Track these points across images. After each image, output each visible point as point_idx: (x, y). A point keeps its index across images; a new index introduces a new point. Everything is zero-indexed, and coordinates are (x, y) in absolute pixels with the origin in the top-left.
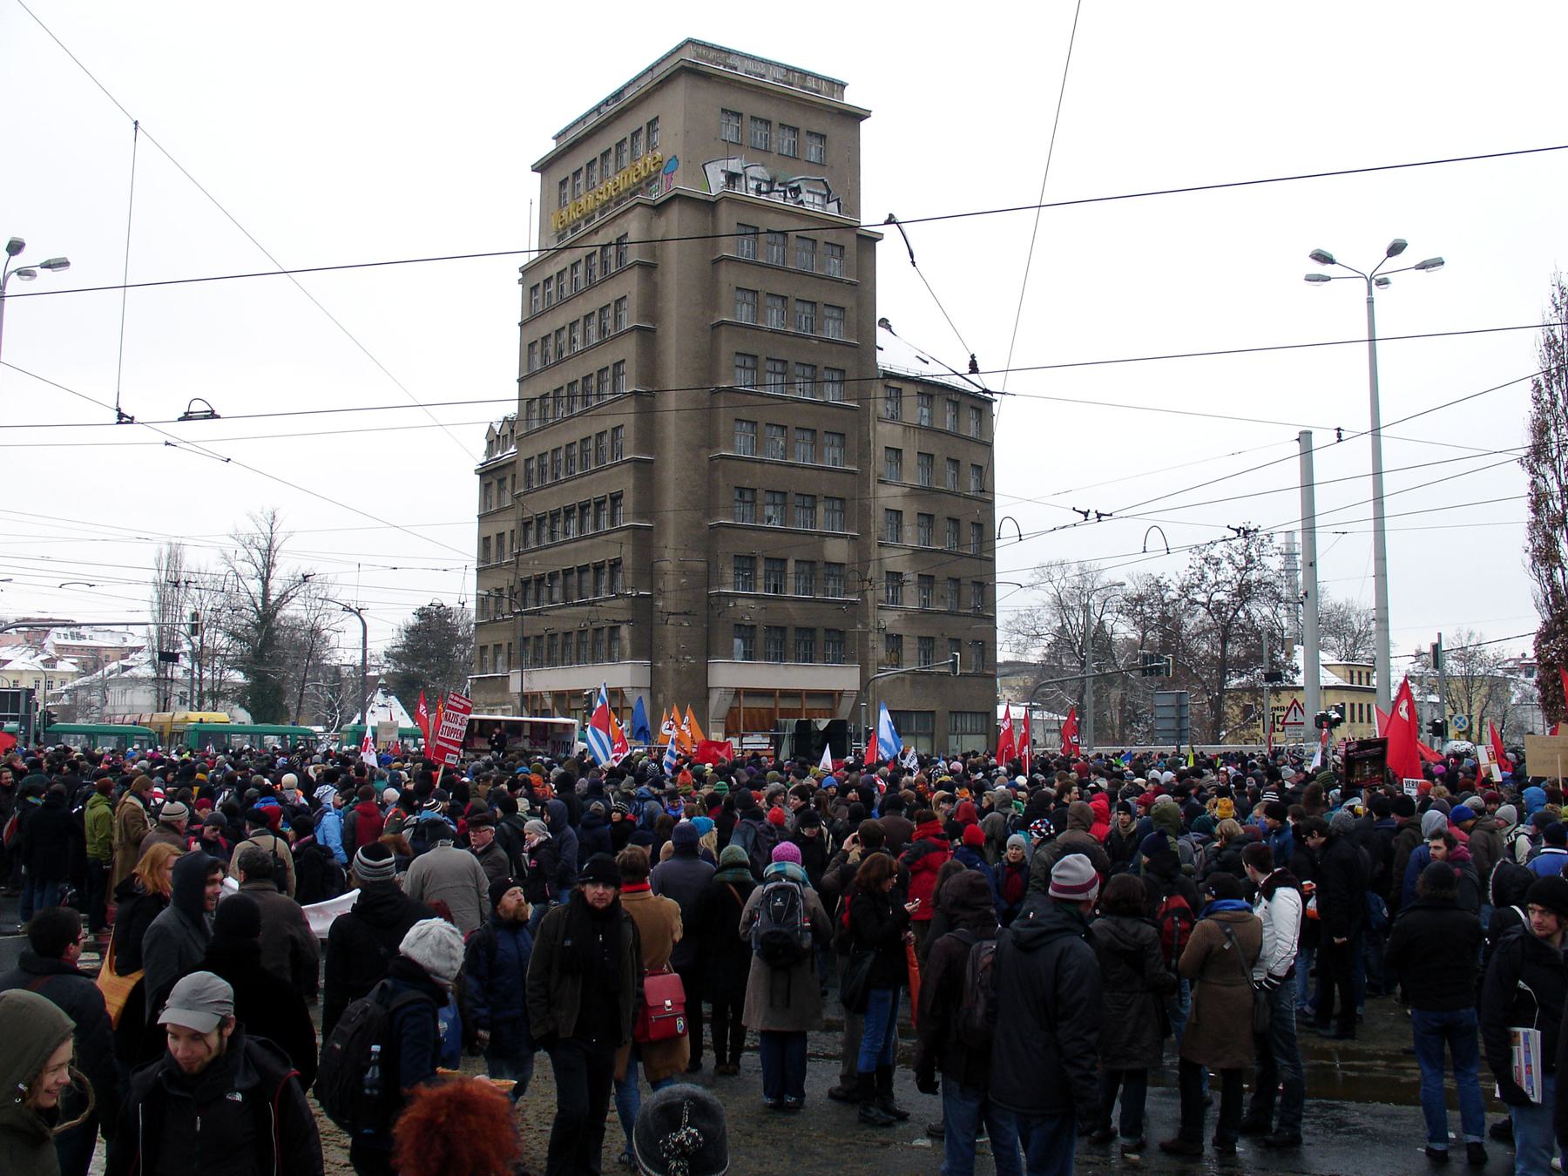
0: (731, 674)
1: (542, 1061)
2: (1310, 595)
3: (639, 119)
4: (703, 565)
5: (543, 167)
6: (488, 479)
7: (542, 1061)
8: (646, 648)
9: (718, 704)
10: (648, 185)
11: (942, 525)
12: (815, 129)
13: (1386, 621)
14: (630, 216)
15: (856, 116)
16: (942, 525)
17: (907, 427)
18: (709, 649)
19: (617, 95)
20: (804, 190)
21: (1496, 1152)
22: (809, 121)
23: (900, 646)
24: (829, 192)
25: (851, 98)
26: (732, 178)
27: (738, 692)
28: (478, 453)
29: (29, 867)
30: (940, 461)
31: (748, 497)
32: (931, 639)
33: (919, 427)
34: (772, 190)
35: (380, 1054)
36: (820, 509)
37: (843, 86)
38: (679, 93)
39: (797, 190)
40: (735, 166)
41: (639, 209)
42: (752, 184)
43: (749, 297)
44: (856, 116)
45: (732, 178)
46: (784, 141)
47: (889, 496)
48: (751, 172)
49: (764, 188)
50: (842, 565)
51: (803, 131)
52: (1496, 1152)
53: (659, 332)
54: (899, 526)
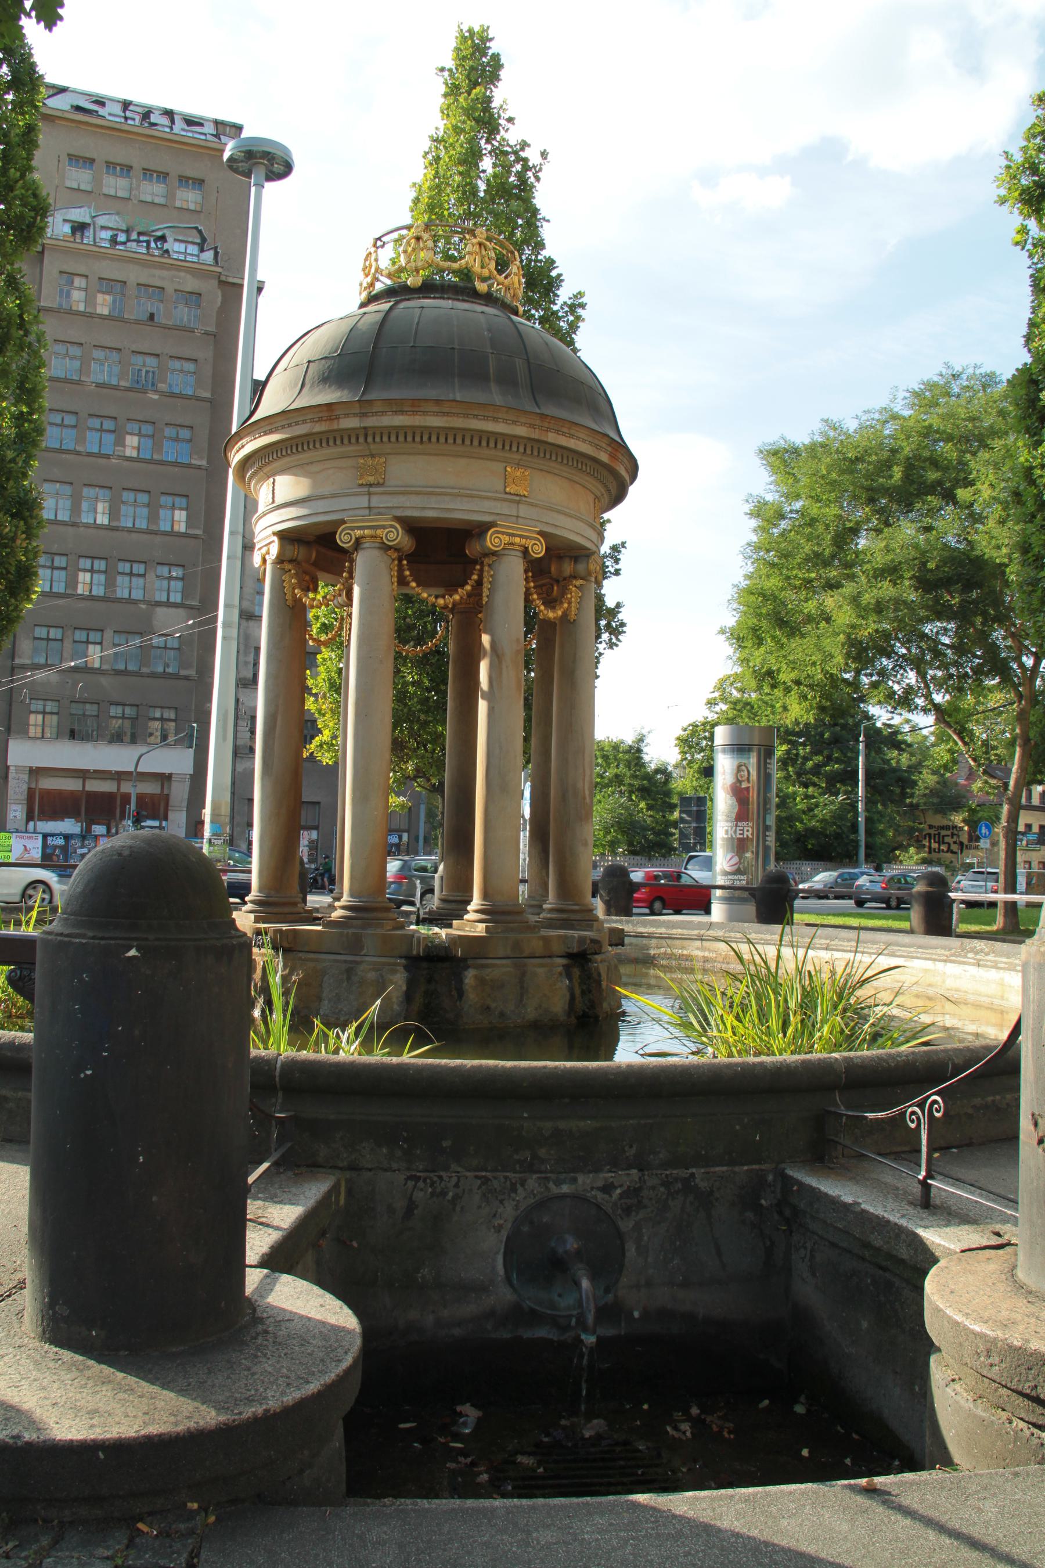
1: (459, 1408)
2: (605, 578)
7: (459, 1408)
12: (189, 173)
13: (118, 773)
20: (170, 239)
21: (3, 1315)
22: (498, 54)
24: (204, 240)
26: (79, 228)
27: (35, 772)
29: (98, 1458)
34: (129, 240)
35: (796, 1402)
39: (163, 239)
40: (80, 215)
42: (106, 235)
43: (115, 355)
48: (102, 221)
49: (122, 238)
52: (3, 1315)
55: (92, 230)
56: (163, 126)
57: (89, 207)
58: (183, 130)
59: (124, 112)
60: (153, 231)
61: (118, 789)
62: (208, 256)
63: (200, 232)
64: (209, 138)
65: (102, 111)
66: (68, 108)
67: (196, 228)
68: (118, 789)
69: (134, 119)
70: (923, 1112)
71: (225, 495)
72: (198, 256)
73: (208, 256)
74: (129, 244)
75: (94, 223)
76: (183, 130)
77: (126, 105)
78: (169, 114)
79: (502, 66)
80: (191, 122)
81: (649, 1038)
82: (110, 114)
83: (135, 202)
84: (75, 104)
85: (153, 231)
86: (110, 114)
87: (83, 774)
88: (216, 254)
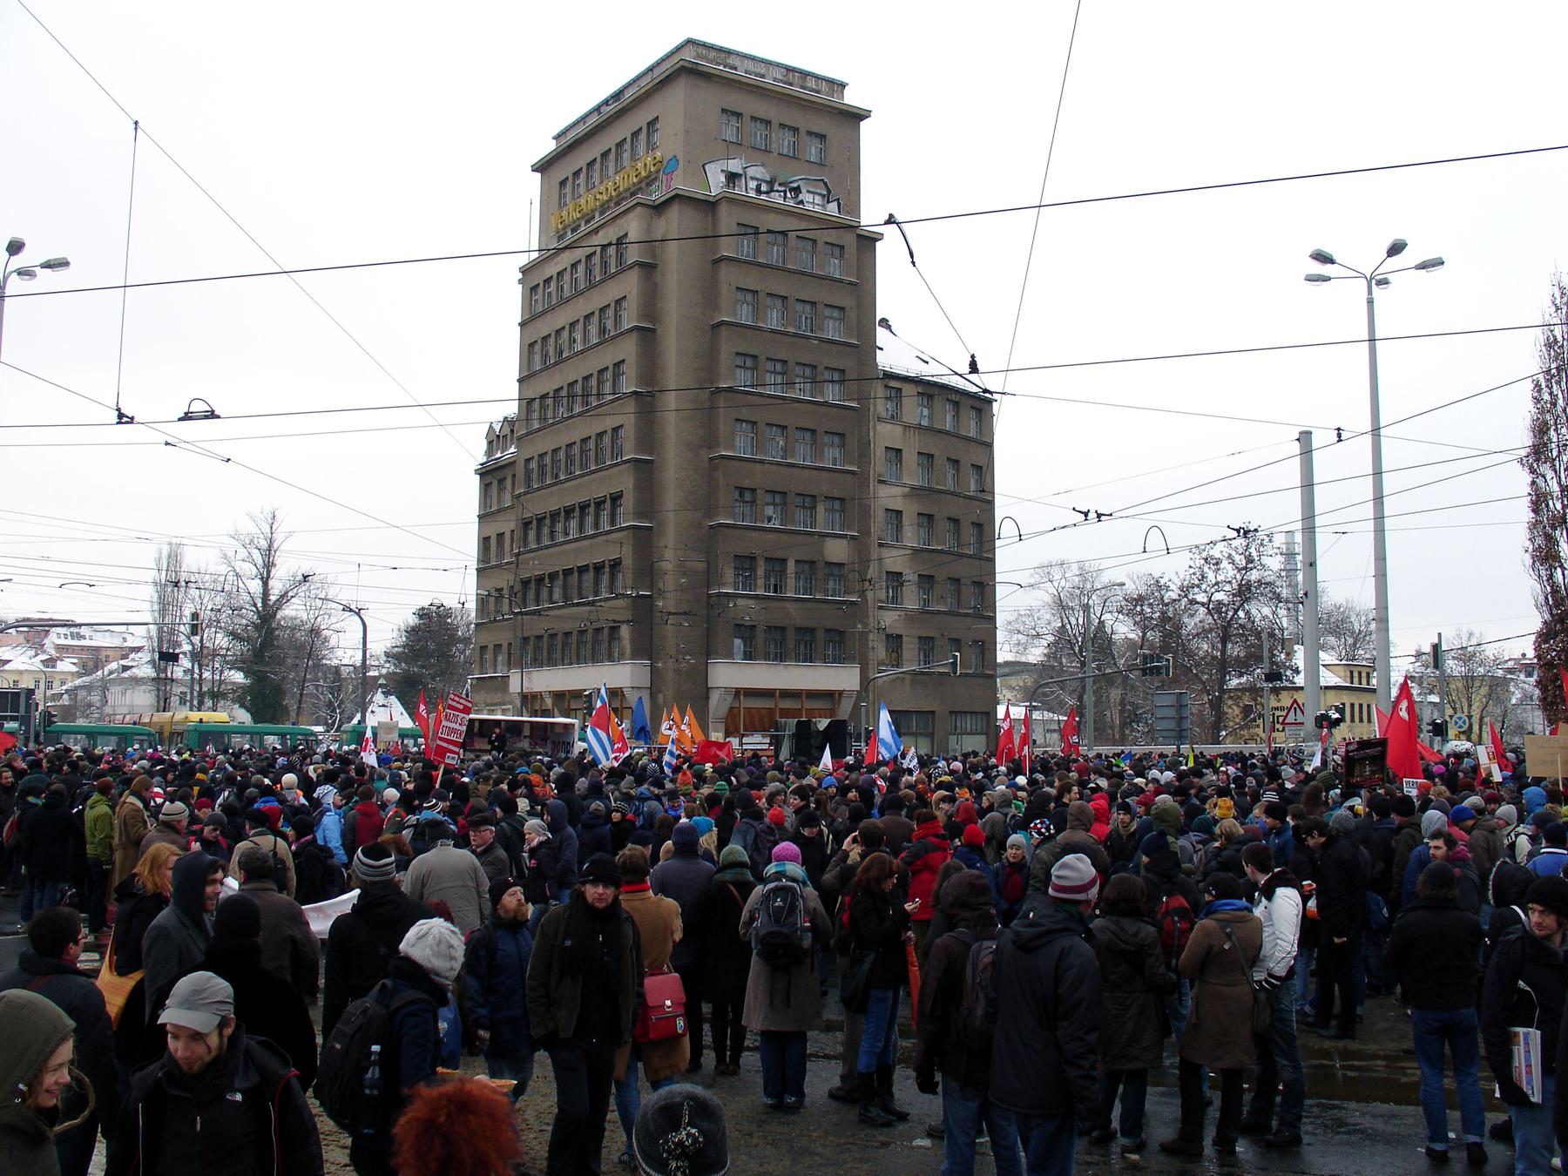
0: (731, 674)
1: (542, 1061)
2: (1310, 595)
3: (639, 119)
4: (703, 565)
5: (543, 167)
7: (542, 1061)
8: (646, 648)
9: (718, 704)
10: (648, 185)
11: (942, 525)
12: (815, 129)
13: (1386, 621)
14: (630, 216)
15: (856, 116)
16: (942, 525)
17: (907, 427)
18: (709, 649)
19: (617, 95)
20: (804, 190)
21: (1496, 1152)
22: (809, 121)
23: (900, 646)
24: (829, 192)
25: (851, 98)
26: (732, 178)
27: (738, 692)
29: (29, 867)
30: (940, 461)
31: (748, 497)
32: (931, 639)
33: (919, 427)
34: (772, 190)
35: (380, 1054)
36: (820, 509)
37: (843, 86)
38: (679, 93)
39: (797, 190)
40: (735, 166)
41: (639, 209)
42: (752, 184)
43: (749, 297)
44: (856, 116)
45: (732, 178)
46: (784, 141)
47: (889, 496)
48: (751, 172)
49: (764, 188)
50: (842, 565)
51: (803, 131)
52: (1496, 1152)
53: (659, 332)
54: (899, 526)
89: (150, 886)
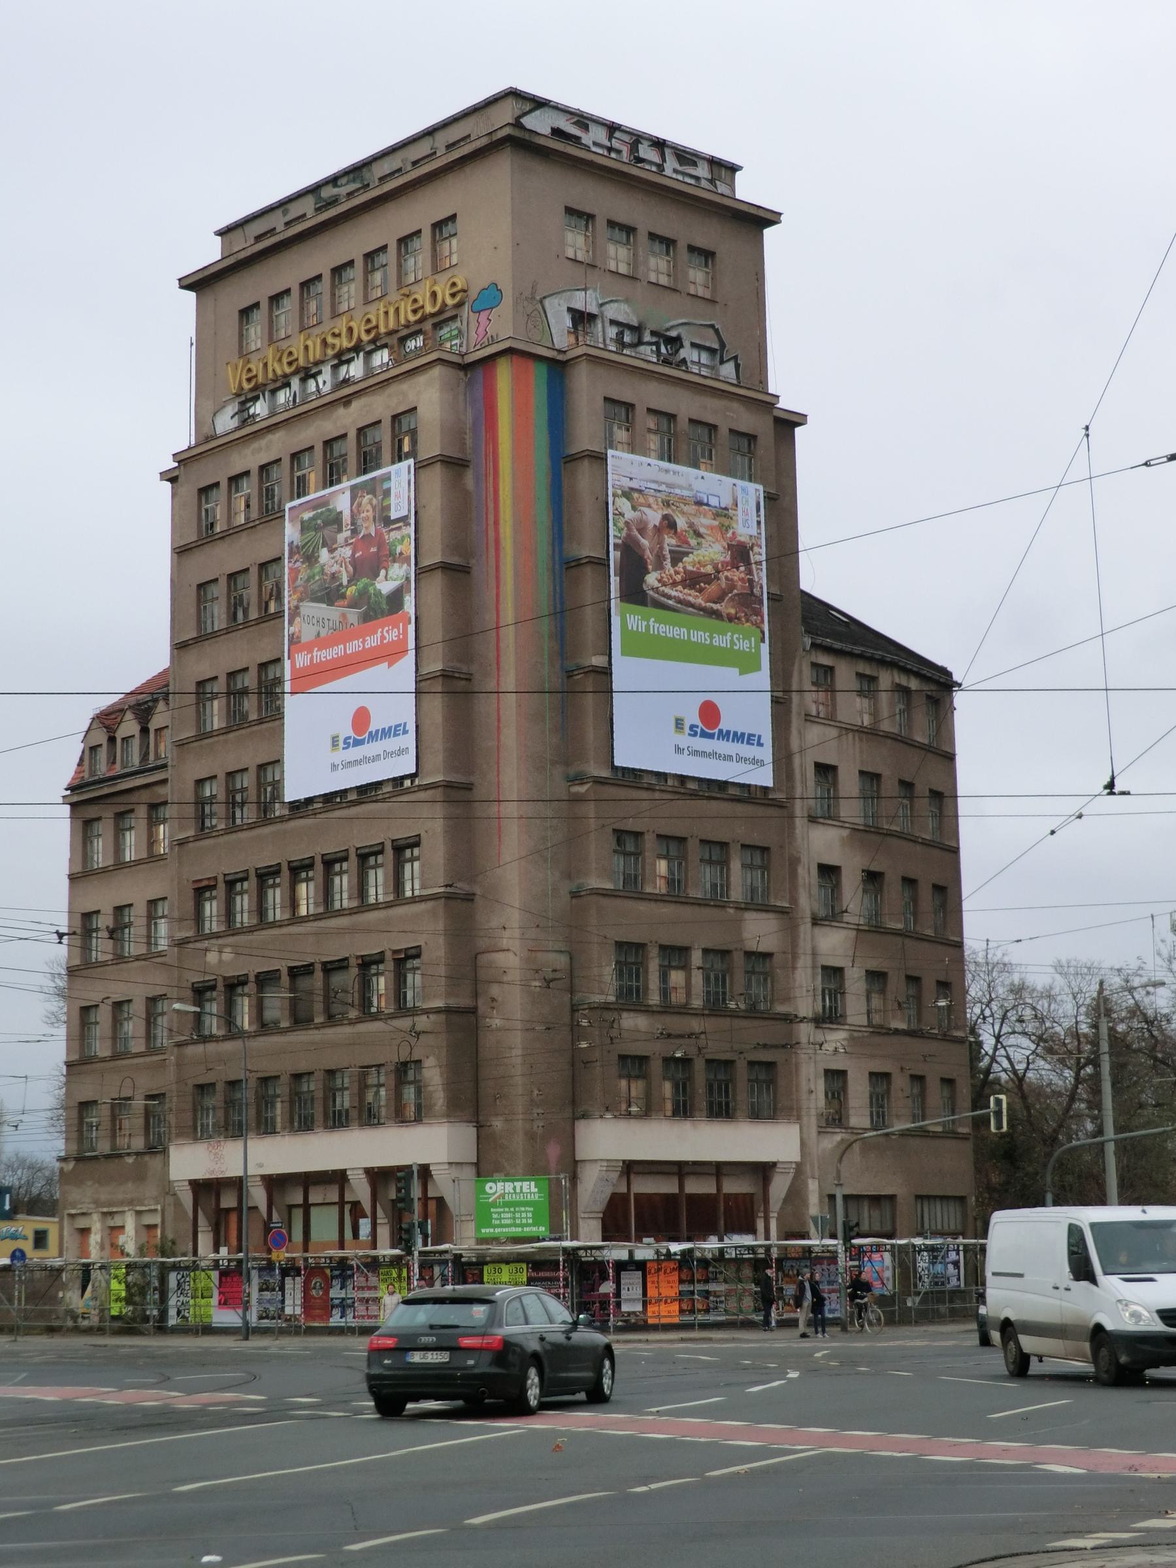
0: (609, 1141)
3: (418, 213)
4: (562, 961)
5: (200, 283)
6: (92, 812)
8: (470, 1101)
9: (594, 1188)
10: (437, 326)
11: (893, 891)
14: (422, 379)
15: (758, 220)
16: (893, 891)
17: (847, 729)
18: (574, 1104)
19: (356, 171)
20: (687, 344)
23: (844, 1088)
25: (748, 189)
26: (581, 319)
27: (630, 1168)
28: (63, 764)
30: (890, 787)
31: (630, 847)
32: (886, 1076)
33: (860, 731)
34: (640, 343)
36: (736, 865)
37: (733, 169)
38: (499, 178)
40: (585, 301)
41: (437, 371)
44: (758, 220)
45: (581, 319)
46: (657, 267)
47: (822, 843)
48: (611, 312)
49: (627, 338)
50: (768, 956)
51: (682, 246)
53: (475, 571)
54: (836, 888)
55: (600, 326)
56: (651, 163)
57: (595, 290)
58: (675, 171)
59: (610, 140)
60: (668, 330)
61: (719, 1189)
62: (728, 370)
63: (717, 331)
64: (704, 184)
65: (587, 139)
66: (546, 131)
67: (712, 326)
68: (719, 1189)
69: (619, 152)
70: (388, 788)
71: (279, 1564)
72: (712, 368)
73: (728, 370)
74: (642, 348)
75: (602, 313)
76: (675, 171)
77: (613, 128)
78: (659, 144)
79: (257, 269)
80: (686, 157)
81: (307, 770)
82: (595, 144)
83: (645, 283)
84: (555, 126)
85: (668, 330)
86: (595, 144)
87: (681, 1170)
88: (737, 366)
89: (952, 1209)
